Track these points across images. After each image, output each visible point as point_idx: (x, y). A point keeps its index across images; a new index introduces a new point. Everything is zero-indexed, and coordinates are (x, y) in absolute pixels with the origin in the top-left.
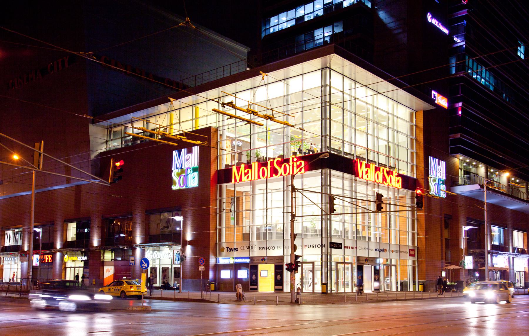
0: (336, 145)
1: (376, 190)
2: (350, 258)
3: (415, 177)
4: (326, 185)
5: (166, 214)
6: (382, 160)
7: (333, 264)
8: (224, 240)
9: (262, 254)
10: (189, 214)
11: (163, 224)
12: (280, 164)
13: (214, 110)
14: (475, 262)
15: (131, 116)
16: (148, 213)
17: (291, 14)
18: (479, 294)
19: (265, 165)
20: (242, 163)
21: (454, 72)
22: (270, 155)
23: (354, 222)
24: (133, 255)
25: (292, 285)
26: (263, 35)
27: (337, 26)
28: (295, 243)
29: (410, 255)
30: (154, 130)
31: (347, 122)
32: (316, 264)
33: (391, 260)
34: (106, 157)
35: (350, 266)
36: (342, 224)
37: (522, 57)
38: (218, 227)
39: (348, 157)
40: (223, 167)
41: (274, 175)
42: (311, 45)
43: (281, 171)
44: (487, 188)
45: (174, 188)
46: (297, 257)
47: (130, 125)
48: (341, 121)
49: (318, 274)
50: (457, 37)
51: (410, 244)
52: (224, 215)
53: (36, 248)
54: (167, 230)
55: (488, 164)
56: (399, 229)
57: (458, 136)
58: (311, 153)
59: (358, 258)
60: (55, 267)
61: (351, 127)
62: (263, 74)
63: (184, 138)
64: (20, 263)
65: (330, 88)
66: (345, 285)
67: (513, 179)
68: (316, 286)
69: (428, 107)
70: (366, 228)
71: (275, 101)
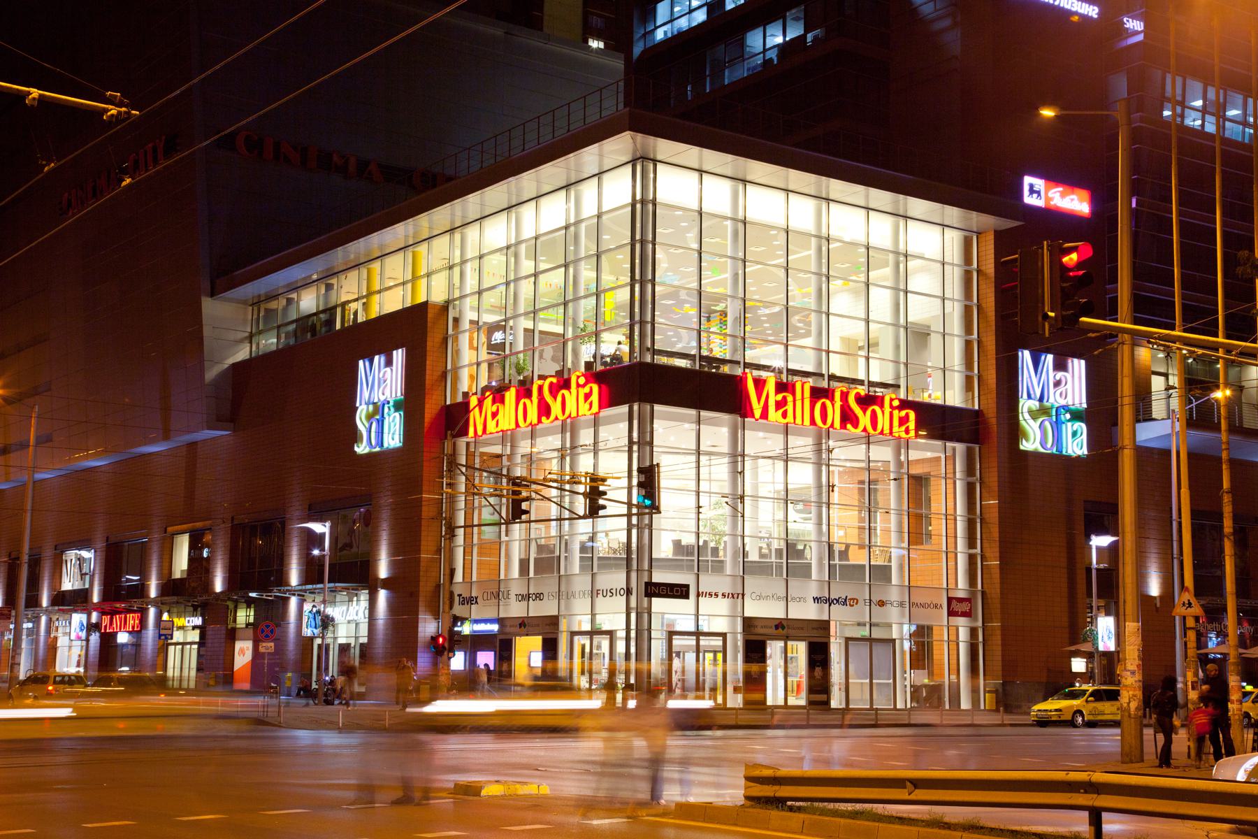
3: (976, 407)
23: (739, 532)
41: (544, 419)
45: (361, 449)
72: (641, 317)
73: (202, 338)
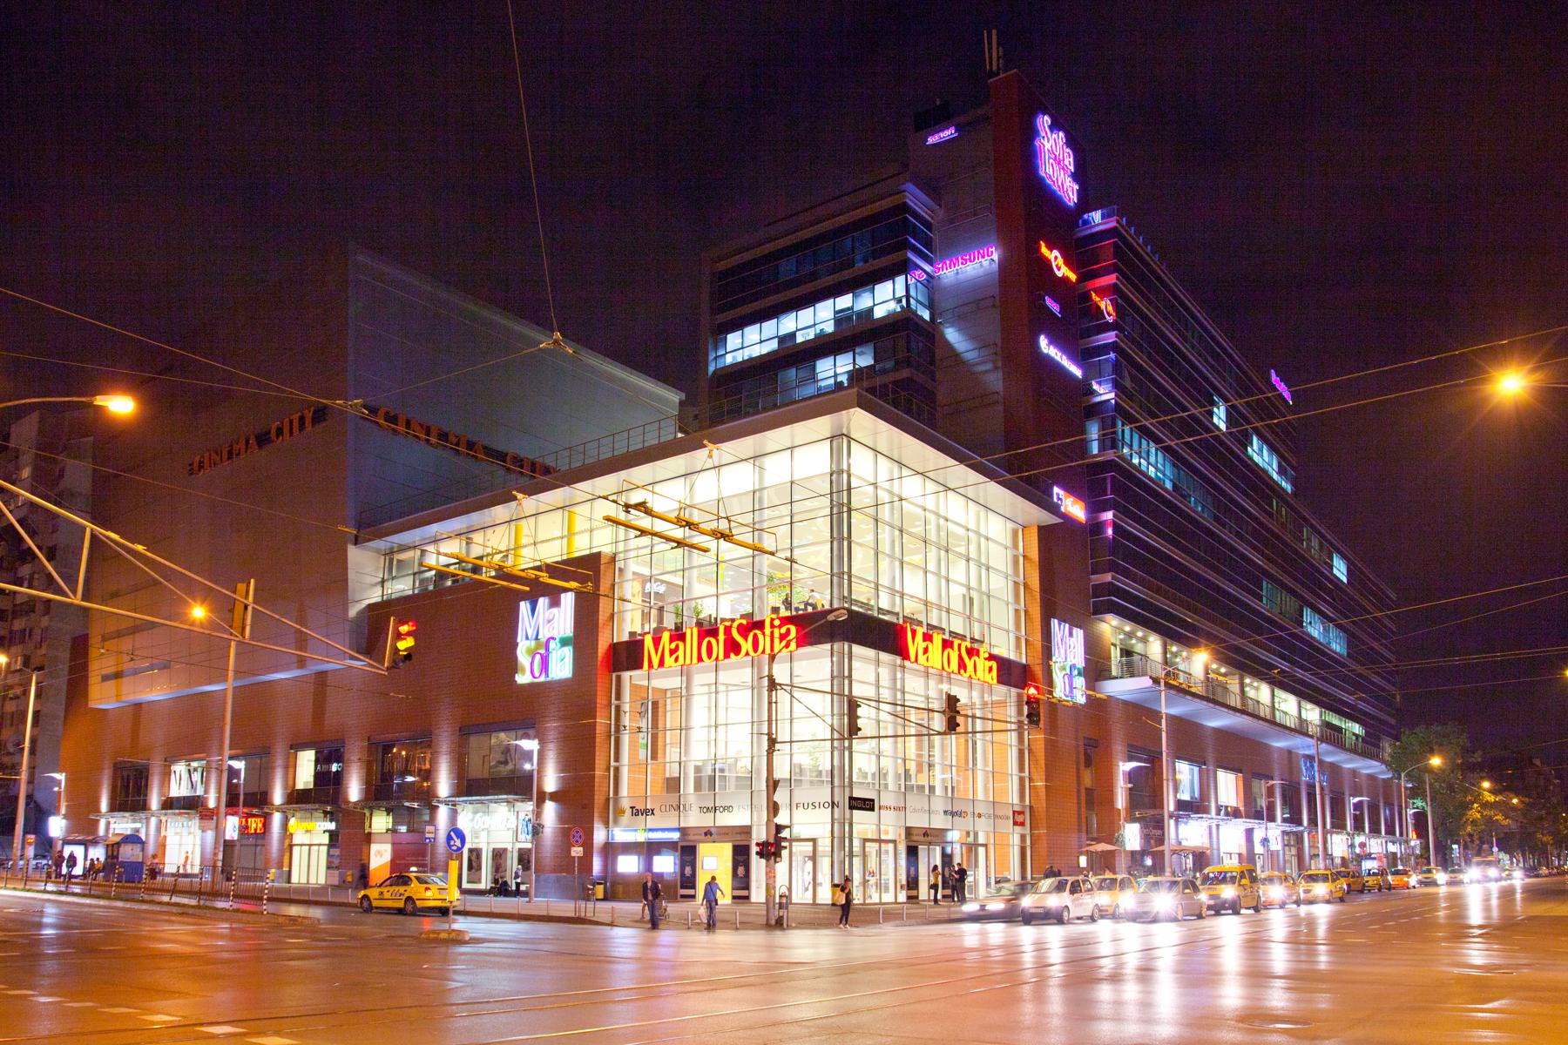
0: (862, 593)
1: (945, 687)
2: (890, 829)
4: (841, 676)
5: (502, 735)
6: (957, 625)
7: (856, 843)
8: (624, 791)
9: (706, 821)
10: (552, 735)
11: (496, 756)
12: (744, 631)
13: (608, 519)
14: (1146, 838)
15: (434, 529)
16: (465, 732)
17: (769, 327)
18: (1143, 902)
19: (713, 632)
20: (665, 629)
21: (1095, 451)
22: (725, 613)
23: (900, 754)
24: (432, 821)
25: (770, 888)
26: (711, 369)
27: (861, 354)
28: (776, 798)
29: (1015, 823)
30: (481, 558)
31: (885, 546)
32: (820, 842)
33: (976, 835)
34: (379, 615)
35: (891, 846)
36: (874, 758)
37: (1223, 427)
38: (613, 763)
39: (886, 618)
40: (626, 638)
42: (810, 390)
43: (746, 645)
44: (1166, 684)
45: (522, 679)
46: (779, 828)
47: (431, 548)
48: (872, 545)
49: (824, 864)
50: (1099, 383)
51: (1016, 800)
52: (626, 739)
53: (232, 803)
54: (505, 770)
55: (1168, 635)
56: (992, 771)
57: (1108, 577)
58: (810, 609)
59: (909, 831)
60: (270, 843)
61: (892, 557)
62: (711, 446)
63: (544, 577)
64: (199, 832)
65: (849, 476)
66: (881, 887)
67: (1214, 666)
68: (819, 889)
69: (1048, 519)
70: (926, 768)
71: (734, 501)
73: (346, 580)
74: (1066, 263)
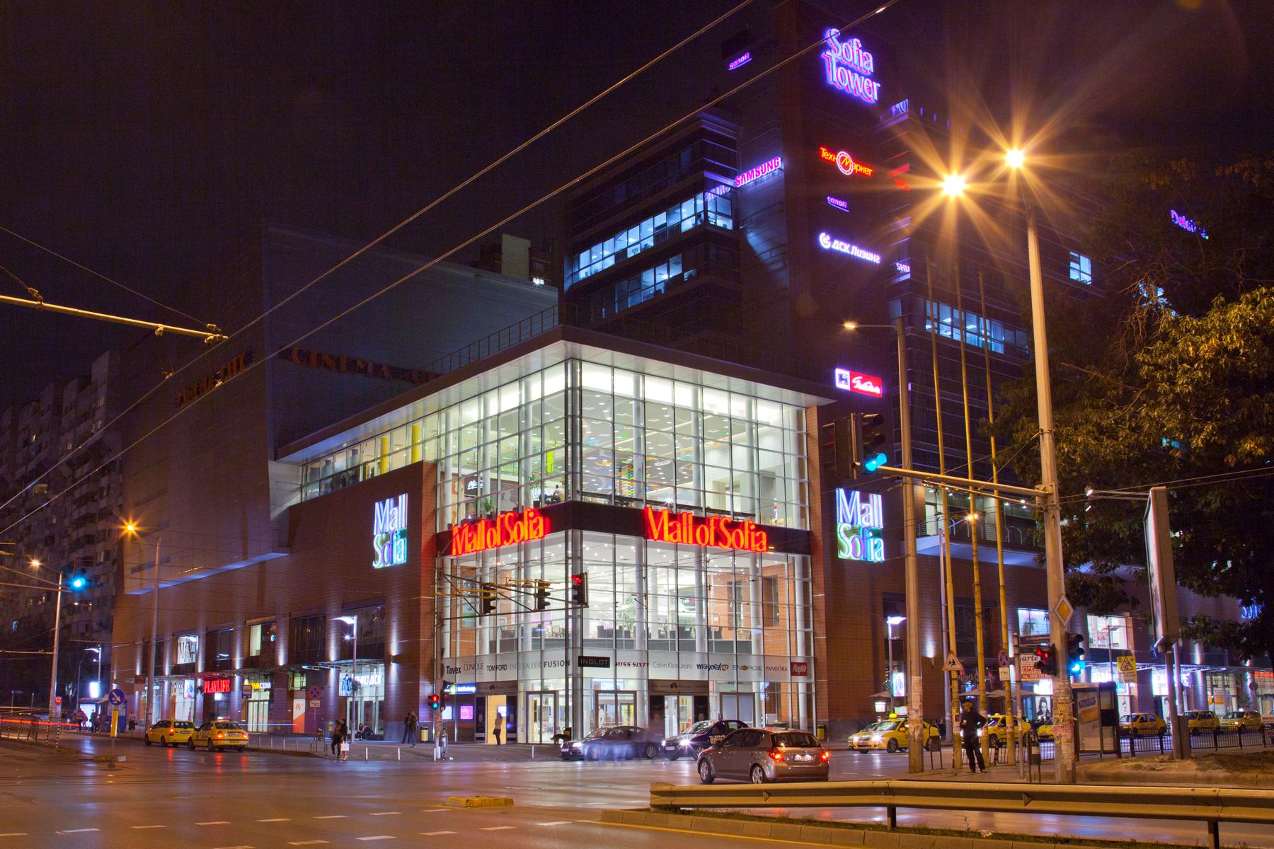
45: (377, 565)
72: (573, 468)
73: (268, 488)
74: (856, 161)
